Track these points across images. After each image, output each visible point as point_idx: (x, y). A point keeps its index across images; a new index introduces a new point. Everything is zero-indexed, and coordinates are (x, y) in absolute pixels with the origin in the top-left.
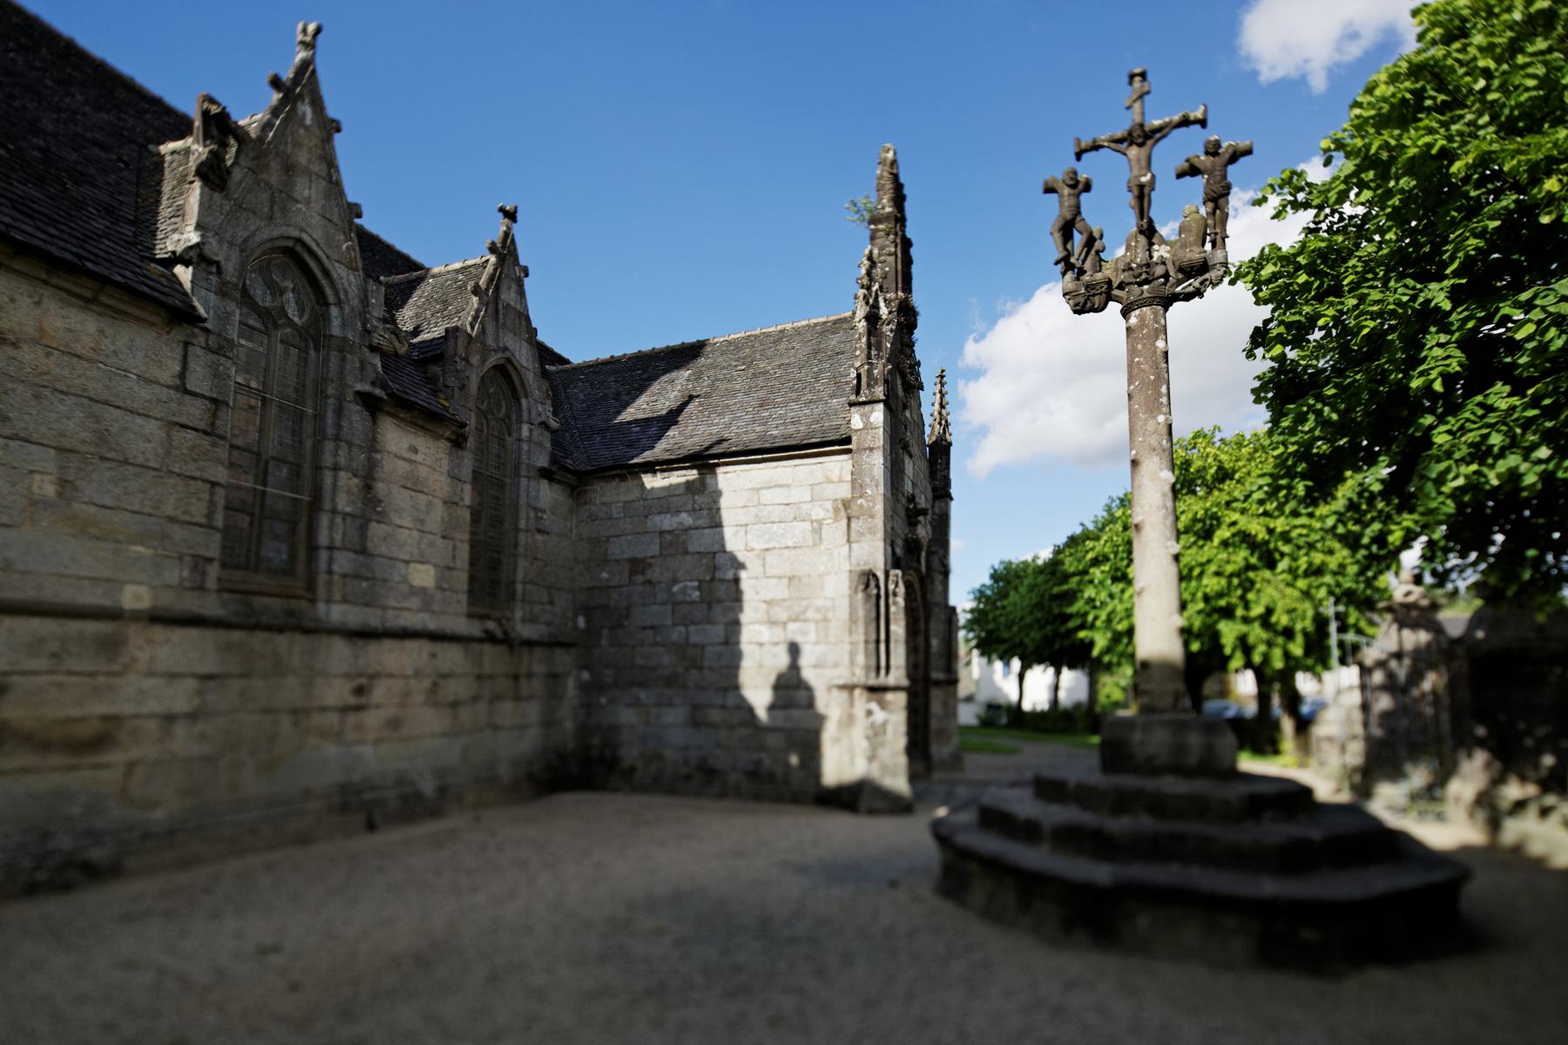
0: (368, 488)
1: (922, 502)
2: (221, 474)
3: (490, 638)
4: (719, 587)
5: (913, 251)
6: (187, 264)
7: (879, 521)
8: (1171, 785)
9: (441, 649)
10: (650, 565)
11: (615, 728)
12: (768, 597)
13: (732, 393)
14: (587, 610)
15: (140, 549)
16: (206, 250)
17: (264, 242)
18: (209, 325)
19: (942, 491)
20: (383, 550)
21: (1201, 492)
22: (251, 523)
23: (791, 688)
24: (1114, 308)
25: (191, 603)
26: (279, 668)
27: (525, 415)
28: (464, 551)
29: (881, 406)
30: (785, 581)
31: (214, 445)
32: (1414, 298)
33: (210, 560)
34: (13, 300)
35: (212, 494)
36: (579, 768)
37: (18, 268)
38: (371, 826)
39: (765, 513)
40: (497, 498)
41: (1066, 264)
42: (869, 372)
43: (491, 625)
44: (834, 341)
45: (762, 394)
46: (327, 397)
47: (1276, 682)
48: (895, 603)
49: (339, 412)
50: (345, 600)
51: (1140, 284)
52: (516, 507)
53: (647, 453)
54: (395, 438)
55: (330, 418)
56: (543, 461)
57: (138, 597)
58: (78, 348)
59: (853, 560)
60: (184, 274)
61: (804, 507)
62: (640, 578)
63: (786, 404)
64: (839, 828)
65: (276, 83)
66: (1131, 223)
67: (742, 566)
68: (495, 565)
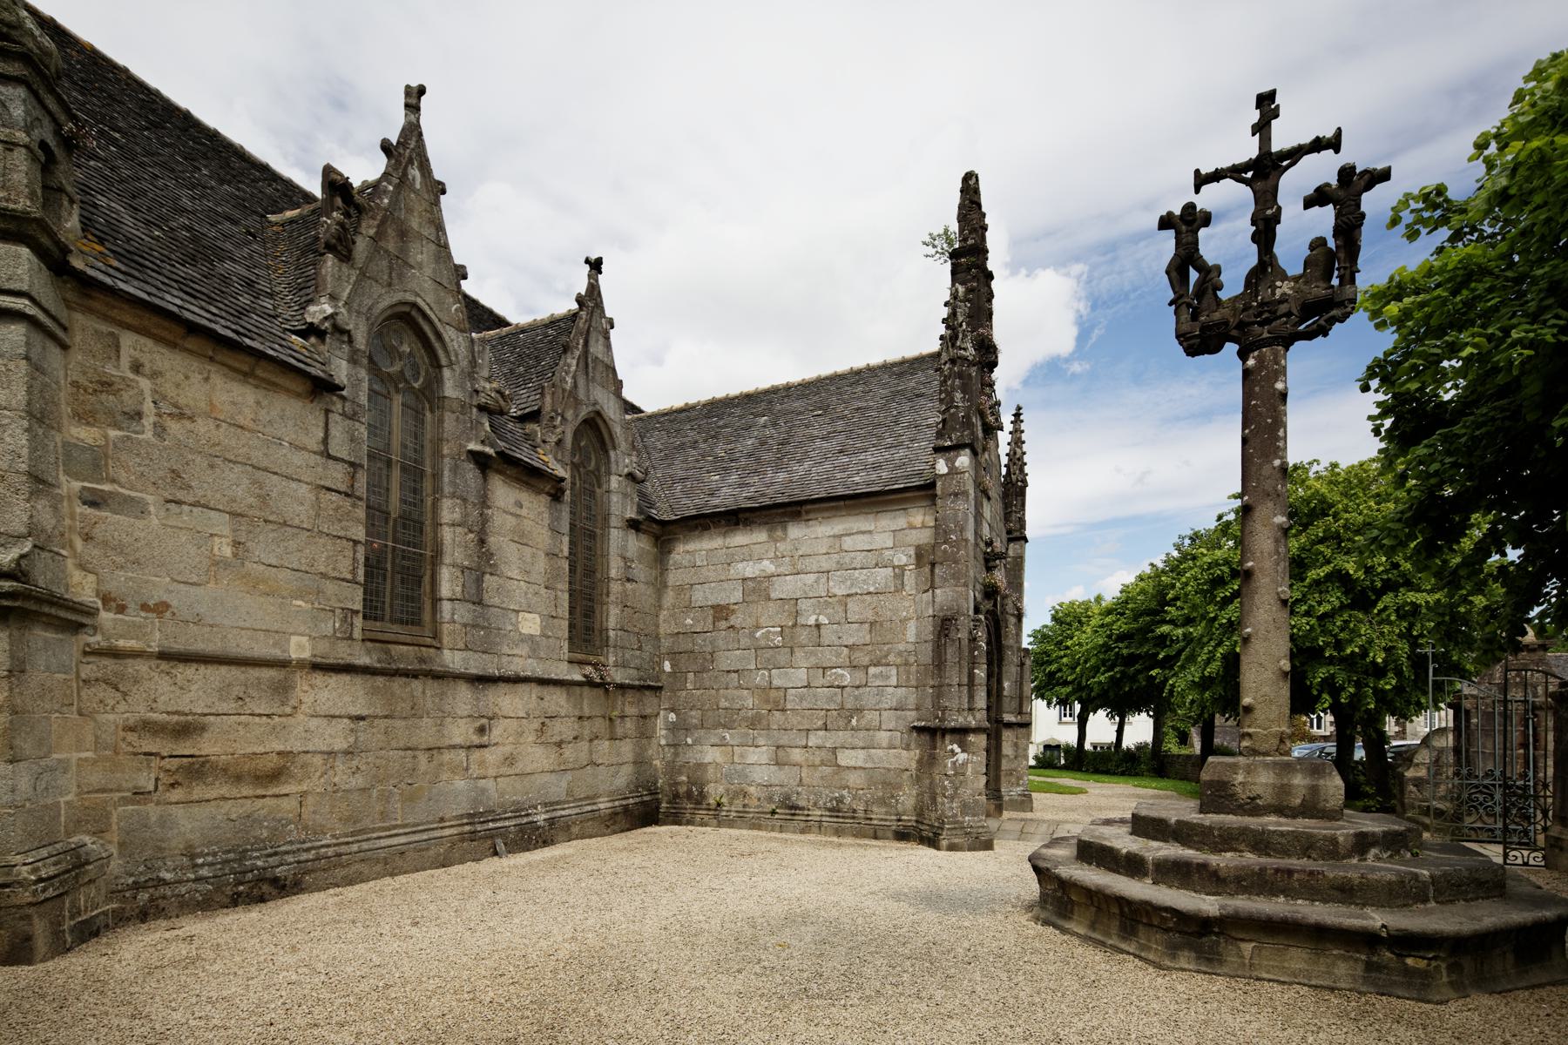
8: (1272, 822)
11: (701, 766)
13: (812, 438)
14: (673, 655)
17: (384, 310)
18: (344, 393)
20: (496, 601)
24: (1231, 349)
26: (415, 713)
27: (613, 467)
34: (187, 378)
35: (355, 552)
37: (189, 346)
38: (496, 854)
39: (847, 560)
40: (590, 549)
43: (589, 669)
46: (443, 456)
49: (455, 470)
50: (467, 648)
54: (504, 494)
57: (300, 647)
58: (241, 420)
59: (937, 606)
61: (887, 553)
62: (723, 625)
68: (589, 613)
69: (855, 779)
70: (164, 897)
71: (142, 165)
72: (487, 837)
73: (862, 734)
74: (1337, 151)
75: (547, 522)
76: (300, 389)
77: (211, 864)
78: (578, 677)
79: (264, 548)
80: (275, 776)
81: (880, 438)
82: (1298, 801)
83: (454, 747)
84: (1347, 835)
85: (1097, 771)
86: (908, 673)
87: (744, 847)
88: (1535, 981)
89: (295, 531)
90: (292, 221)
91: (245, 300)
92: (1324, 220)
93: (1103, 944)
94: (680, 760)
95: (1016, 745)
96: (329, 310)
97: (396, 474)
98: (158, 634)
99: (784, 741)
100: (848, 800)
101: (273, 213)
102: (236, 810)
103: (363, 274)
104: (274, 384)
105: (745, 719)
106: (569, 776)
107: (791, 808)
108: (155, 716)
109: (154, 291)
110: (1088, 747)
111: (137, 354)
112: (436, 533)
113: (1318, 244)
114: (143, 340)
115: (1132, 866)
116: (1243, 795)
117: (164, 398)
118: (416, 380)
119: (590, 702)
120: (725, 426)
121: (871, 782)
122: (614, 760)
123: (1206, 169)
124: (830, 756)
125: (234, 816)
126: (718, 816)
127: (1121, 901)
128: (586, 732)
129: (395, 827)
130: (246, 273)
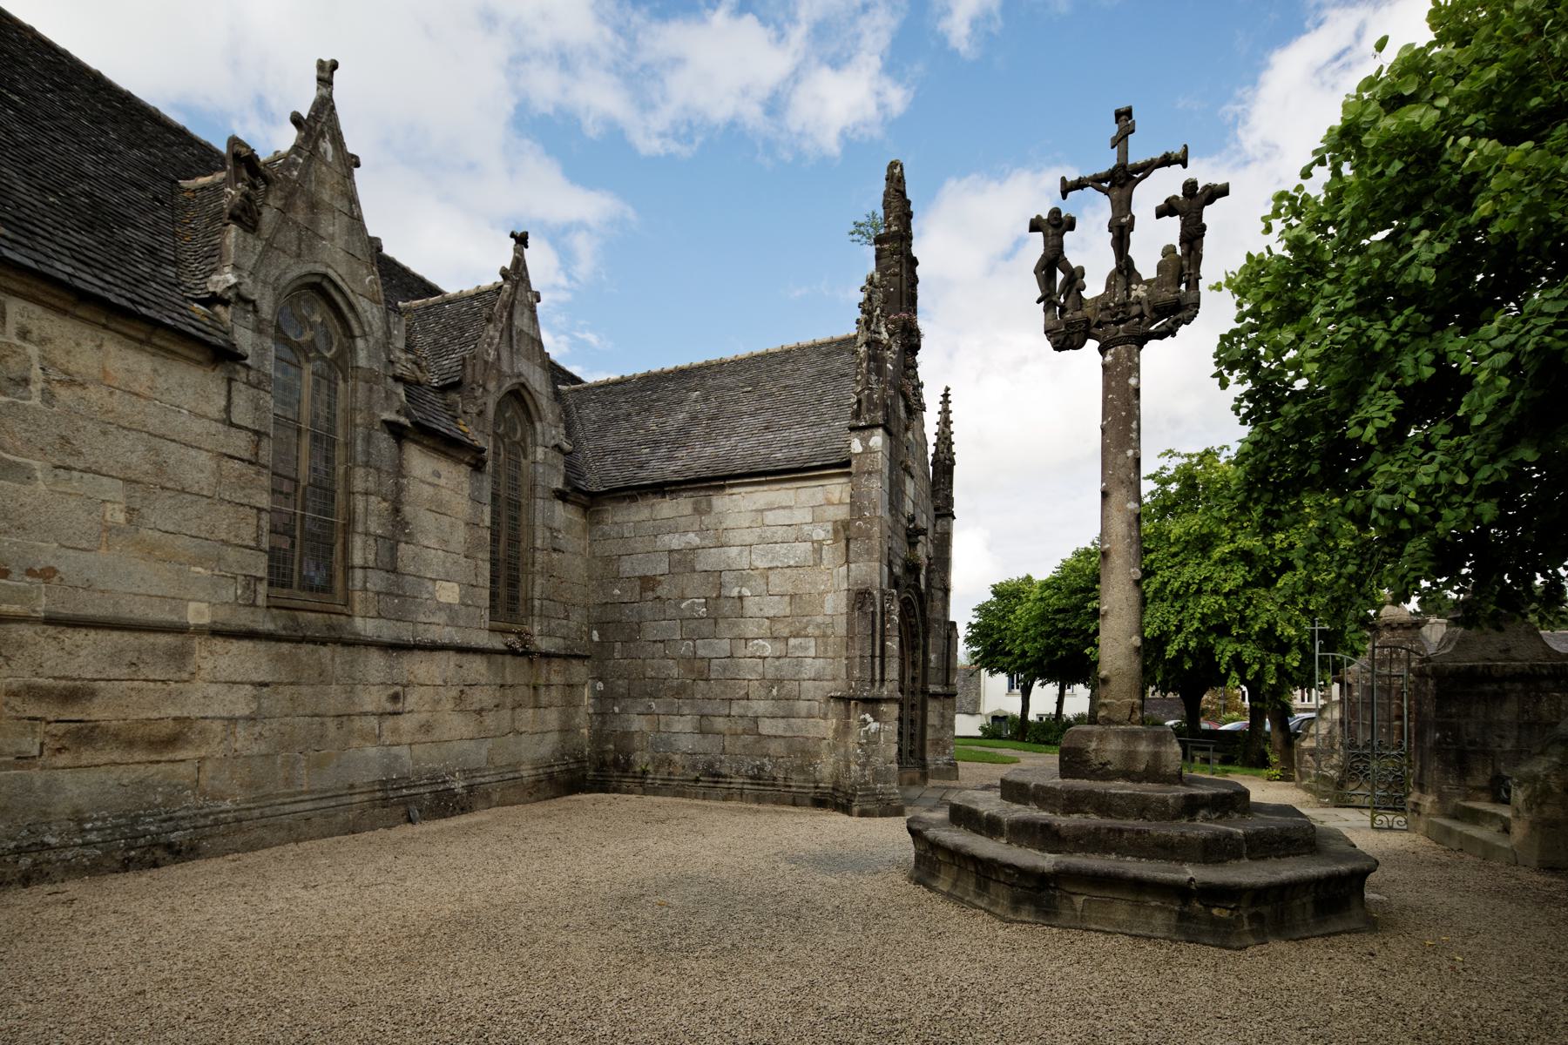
0: (397, 511)
1: (923, 521)
3: (512, 651)
9: (465, 659)
10: (660, 582)
11: (628, 735)
12: (771, 613)
13: (740, 414)
14: (601, 625)
15: (199, 569)
16: (243, 289)
18: (248, 362)
19: (944, 511)
20: (412, 569)
24: (1092, 345)
25: (244, 619)
26: (323, 678)
27: (540, 439)
30: (787, 599)
31: (127, 385)
33: (261, 579)
34: (78, 344)
38: (410, 820)
43: (511, 638)
44: (838, 363)
46: (356, 426)
49: (368, 440)
50: (379, 616)
51: (1117, 323)
52: (532, 526)
54: (420, 463)
56: (558, 484)
57: (199, 613)
58: (136, 388)
61: (806, 528)
62: (650, 595)
68: (513, 583)
69: (775, 748)
70: (48, 862)
71: (42, 128)
72: (398, 804)
73: (783, 703)
74: (1185, 166)
75: (467, 492)
76: (200, 358)
77: (99, 830)
78: (502, 647)
79: (161, 515)
81: (804, 415)
82: (1143, 767)
83: (365, 714)
84: (1177, 798)
85: (1038, 742)
86: (826, 645)
87: (662, 814)
88: (1331, 929)
90: (203, 188)
91: (144, 269)
92: (1171, 229)
93: (962, 900)
94: (607, 729)
95: (942, 716)
96: (233, 280)
97: (306, 442)
98: (44, 600)
99: (708, 709)
100: (769, 768)
101: (188, 178)
102: (128, 775)
103: (269, 244)
104: (173, 352)
105: (670, 688)
106: (489, 744)
107: (714, 775)
109: (43, 259)
110: (1032, 717)
111: (24, 321)
112: (348, 502)
113: (1168, 251)
114: (31, 307)
115: (990, 827)
116: (1095, 761)
117: (53, 364)
119: (513, 670)
120: (658, 400)
121: (791, 750)
122: (538, 728)
123: (1072, 177)
124: (751, 725)
125: (125, 781)
126: (643, 784)
127: (974, 859)
128: (509, 701)
129: (301, 793)
130: (147, 240)
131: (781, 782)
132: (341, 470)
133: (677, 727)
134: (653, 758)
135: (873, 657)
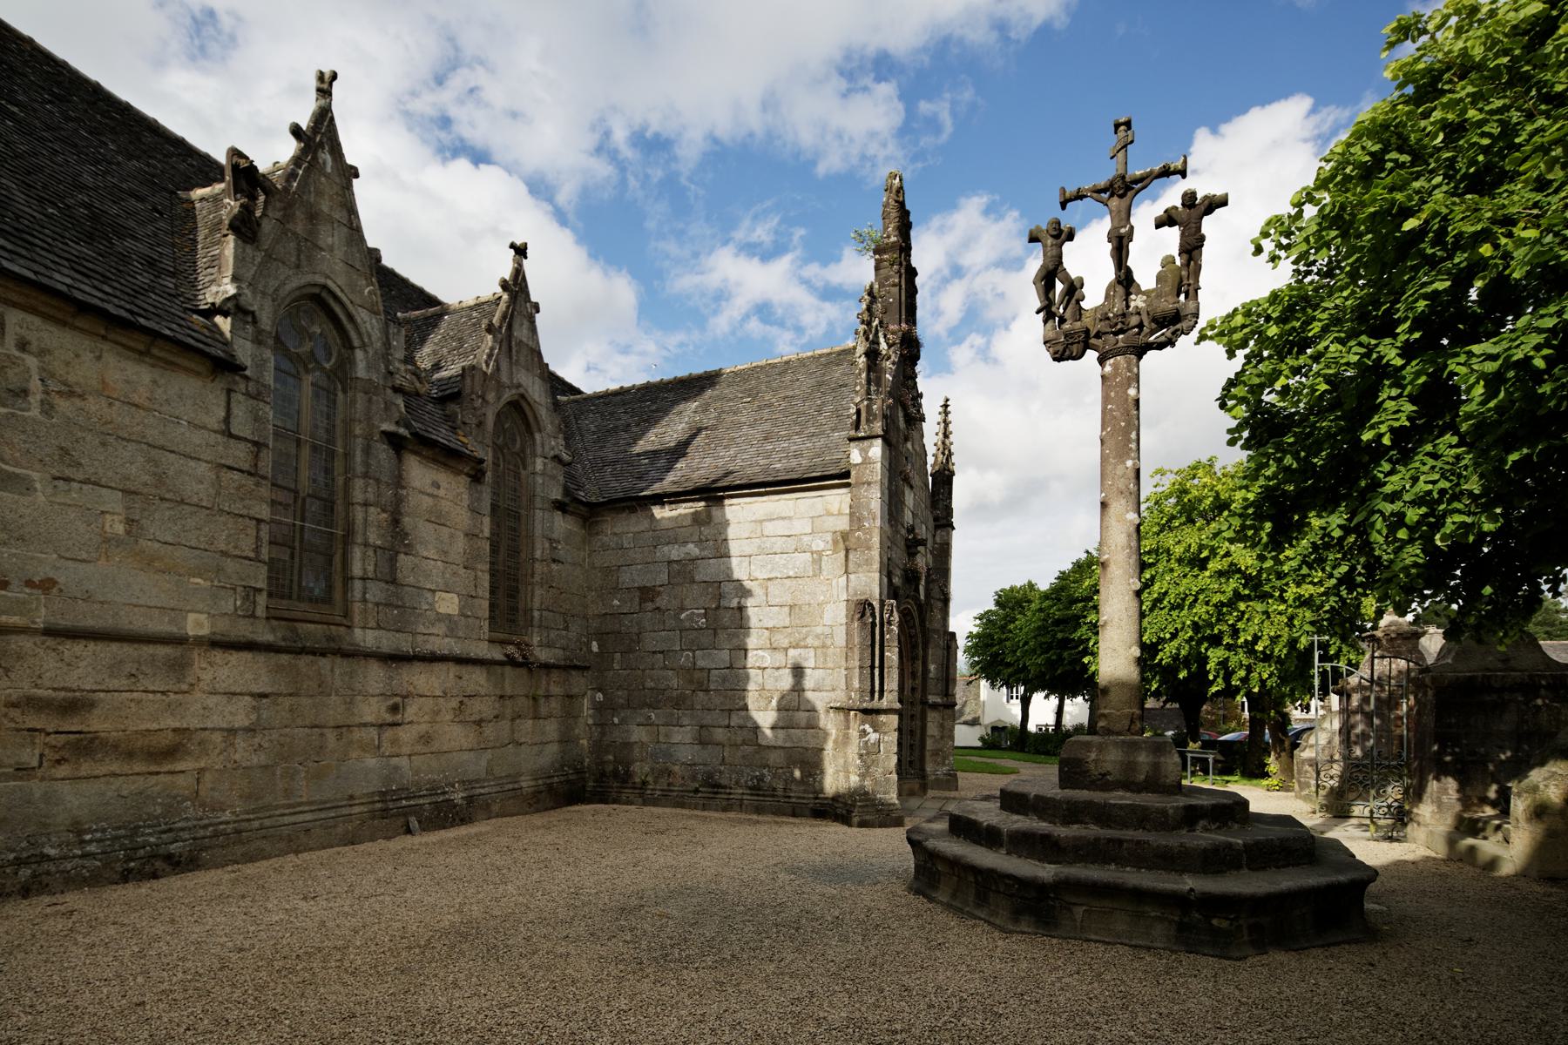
0: (396, 522)
1: (923, 532)
2: (264, 512)
3: (511, 662)
4: (725, 614)
5: (918, 281)
6: (225, 314)
7: (875, 554)
9: (465, 671)
11: (627, 745)
13: (740, 425)
14: (601, 636)
18: (247, 373)
19: (944, 522)
20: (411, 580)
21: (1200, 522)
22: (292, 556)
23: (794, 706)
24: (1091, 356)
25: (244, 630)
26: (323, 689)
27: (539, 450)
28: (485, 580)
29: (879, 441)
30: (786, 609)
32: (1368, 355)
33: (260, 590)
35: (258, 531)
36: (588, 783)
38: (409, 831)
40: (515, 530)
41: (1047, 311)
42: (869, 407)
43: (511, 649)
44: (837, 373)
45: (767, 426)
46: (355, 436)
47: (1268, 707)
48: (890, 631)
49: (367, 451)
50: (379, 627)
51: (1116, 334)
52: (530, 537)
53: (657, 485)
54: (419, 473)
55: (358, 457)
57: (199, 624)
58: (136, 399)
60: (225, 324)
61: (805, 538)
62: (650, 606)
63: (789, 437)
64: (834, 837)
65: (296, 131)
66: (1109, 273)
67: (747, 593)
68: (513, 593)
70: (48, 873)
74: (1184, 176)
75: (466, 503)
77: (99, 841)
78: (502, 658)
80: (171, 753)
82: (1142, 777)
83: (365, 725)
85: (1038, 752)
86: (825, 655)
87: (661, 825)
89: (194, 509)
91: (144, 279)
92: (1171, 238)
93: (961, 911)
95: (942, 726)
97: (306, 452)
98: (43, 610)
99: (708, 720)
102: (128, 787)
103: (269, 256)
104: (172, 363)
106: (488, 755)
108: (40, 692)
109: (42, 270)
111: (23, 332)
113: (1168, 261)
114: (30, 318)
117: (52, 376)
118: (328, 360)
119: (513, 681)
123: (1071, 190)
124: (751, 736)
125: (125, 793)
128: (508, 711)
129: (300, 804)
130: (147, 252)
131: (780, 793)
132: (340, 481)
133: (677, 738)
134: (652, 769)
135: (872, 667)
